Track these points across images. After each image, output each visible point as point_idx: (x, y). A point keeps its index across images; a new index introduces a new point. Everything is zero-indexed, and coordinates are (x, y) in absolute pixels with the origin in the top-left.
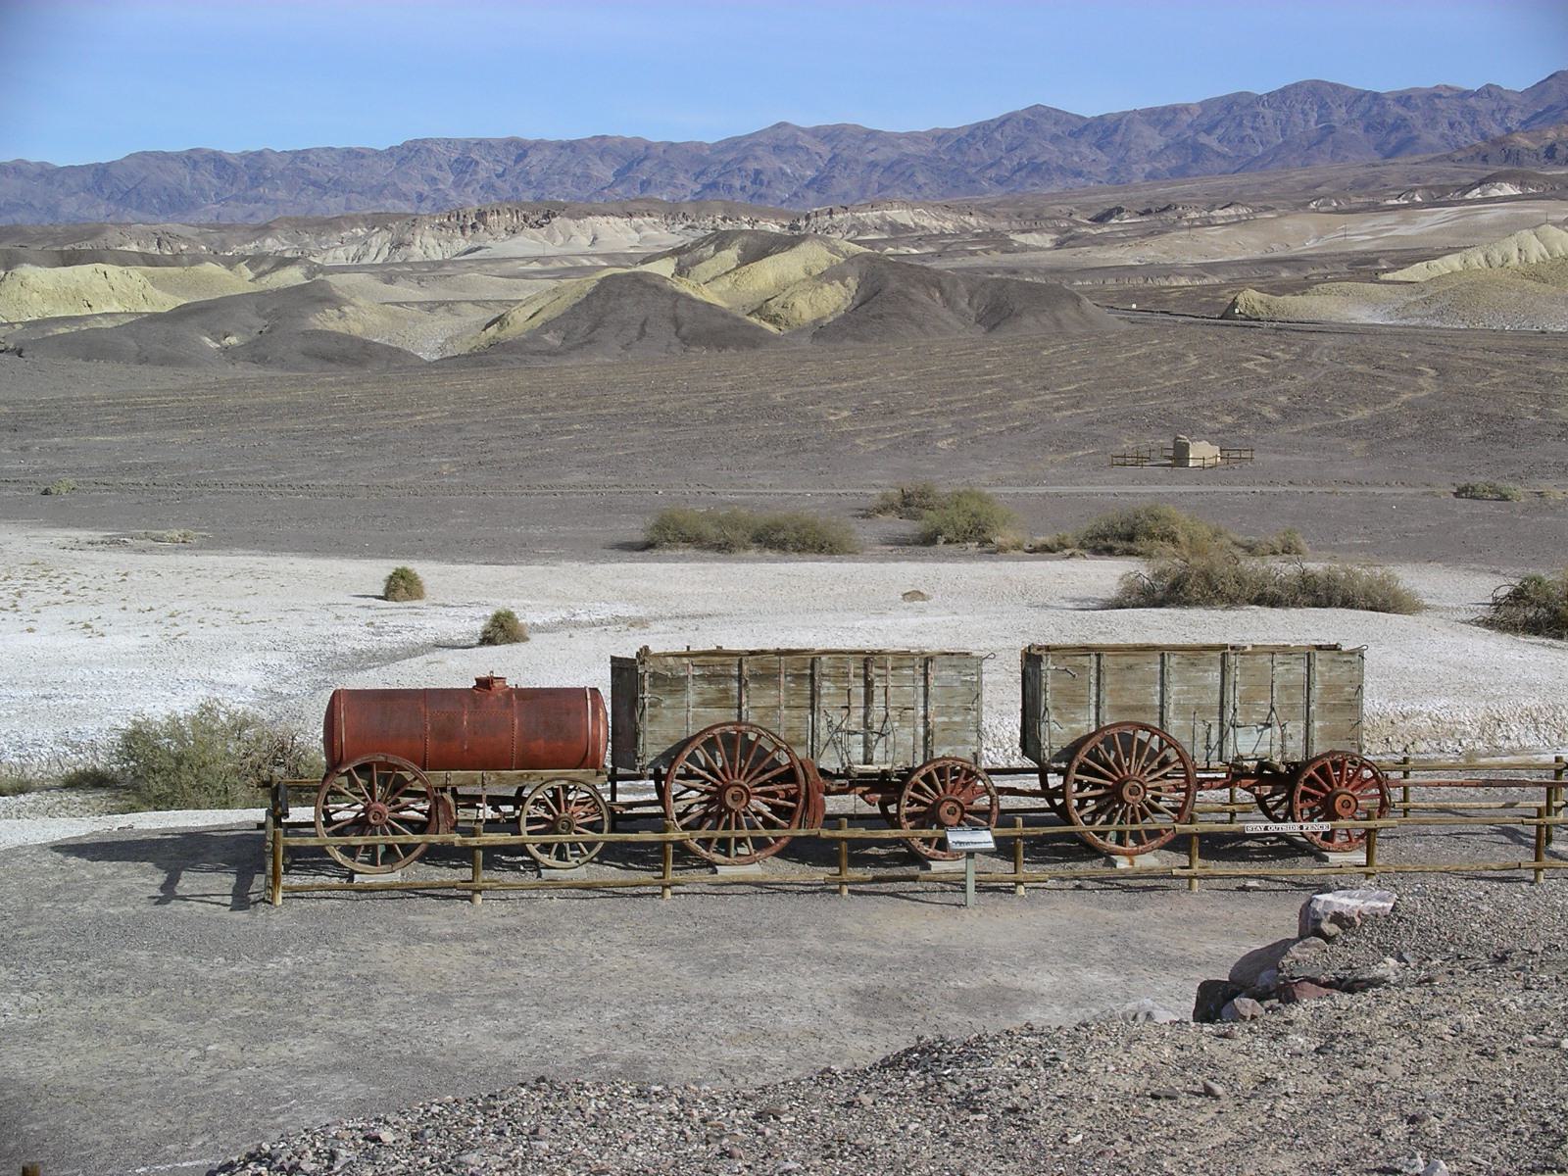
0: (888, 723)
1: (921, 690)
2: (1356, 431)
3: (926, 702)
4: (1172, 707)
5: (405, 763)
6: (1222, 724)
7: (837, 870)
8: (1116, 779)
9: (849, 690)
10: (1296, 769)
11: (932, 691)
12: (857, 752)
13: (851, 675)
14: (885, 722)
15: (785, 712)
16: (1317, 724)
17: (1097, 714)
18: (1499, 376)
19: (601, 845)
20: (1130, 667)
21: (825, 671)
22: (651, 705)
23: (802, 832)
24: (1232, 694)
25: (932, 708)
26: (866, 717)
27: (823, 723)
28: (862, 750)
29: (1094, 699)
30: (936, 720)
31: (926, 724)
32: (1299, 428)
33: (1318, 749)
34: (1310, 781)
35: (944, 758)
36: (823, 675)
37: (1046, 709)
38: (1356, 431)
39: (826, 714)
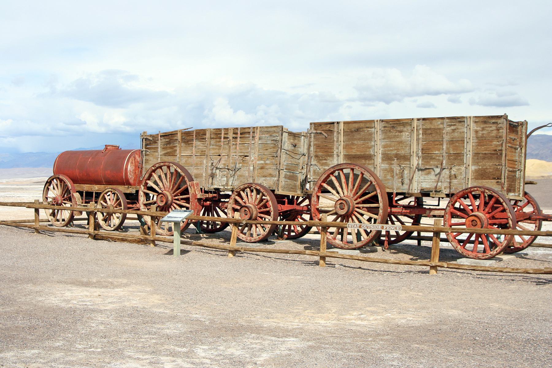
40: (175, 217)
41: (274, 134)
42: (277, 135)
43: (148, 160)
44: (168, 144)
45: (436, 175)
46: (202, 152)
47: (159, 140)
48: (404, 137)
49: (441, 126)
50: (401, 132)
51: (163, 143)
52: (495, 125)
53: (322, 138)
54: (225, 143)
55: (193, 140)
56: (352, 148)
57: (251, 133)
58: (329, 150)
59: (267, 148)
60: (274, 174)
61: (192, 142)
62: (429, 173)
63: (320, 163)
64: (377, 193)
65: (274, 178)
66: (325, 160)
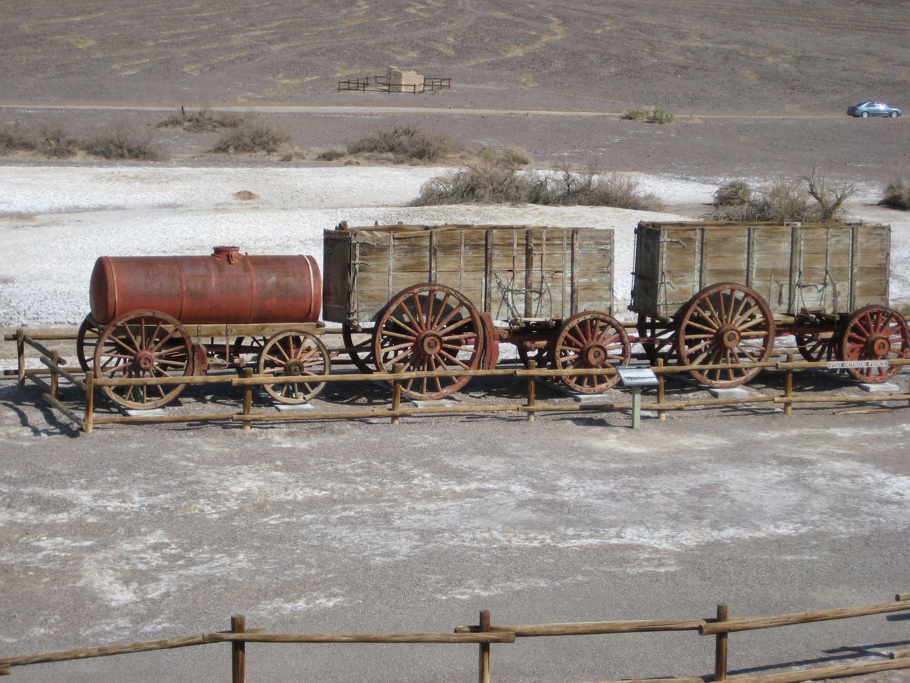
0: (544, 284)
1: (569, 258)
2: (518, 65)
3: (572, 267)
4: (754, 271)
5: (168, 317)
6: (790, 284)
7: (525, 401)
8: (714, 331)
9: (514, 257)
10: (845, 319)
11: (577, 257)
12: (521, 307)
13: (515, 245)
14: (542, 282)
15: (464, 275)
16: (858, 284)
17: (701, 277)
18: (609, 25)
19: (323, 384)
20: (725, 239)
21: (496, 242)
22: (360, 271)
23: (481, 372)
24: (798, 260)
25: (576, 271)
26: (527, 278)
27: (494, 284)
28: (523, 305)
29: (699, 265)
30: (581, 281)
31: (572, 286)
32: (473, 62)
33: (860, 303)
34: (855, 329)
35: (586, 313)
36: (494, 245)
37: (663, 273)
38: (518, 65)
39: (497, 277)
45: (819, 292)
48: (782, 248)
50: (779, 242)
52: (880, 237)
53: (679, 248)
62: (810, 291)
63: (674, 281)
64: (732, 369)
65: (606, 303)
66: (682, 276)
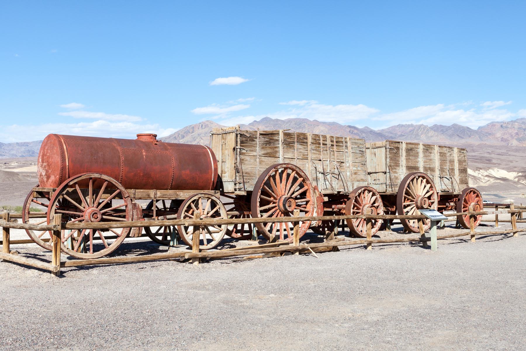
40: (435, 216)
41: (361, 146)
42: (363, 146)
43: (243, 160)
44: (269, 143)
46: (304, 155)
47: (258, 138)
49: (446, 152)
51: (262, 142)
54: (324, 149)
55: (294, 142)
56: (409, 162)
57: (344, 143)
58: (397, 162)
59: (357, 157)
60: (365, 179)
61: (293, 145)
66: (395, 169)
